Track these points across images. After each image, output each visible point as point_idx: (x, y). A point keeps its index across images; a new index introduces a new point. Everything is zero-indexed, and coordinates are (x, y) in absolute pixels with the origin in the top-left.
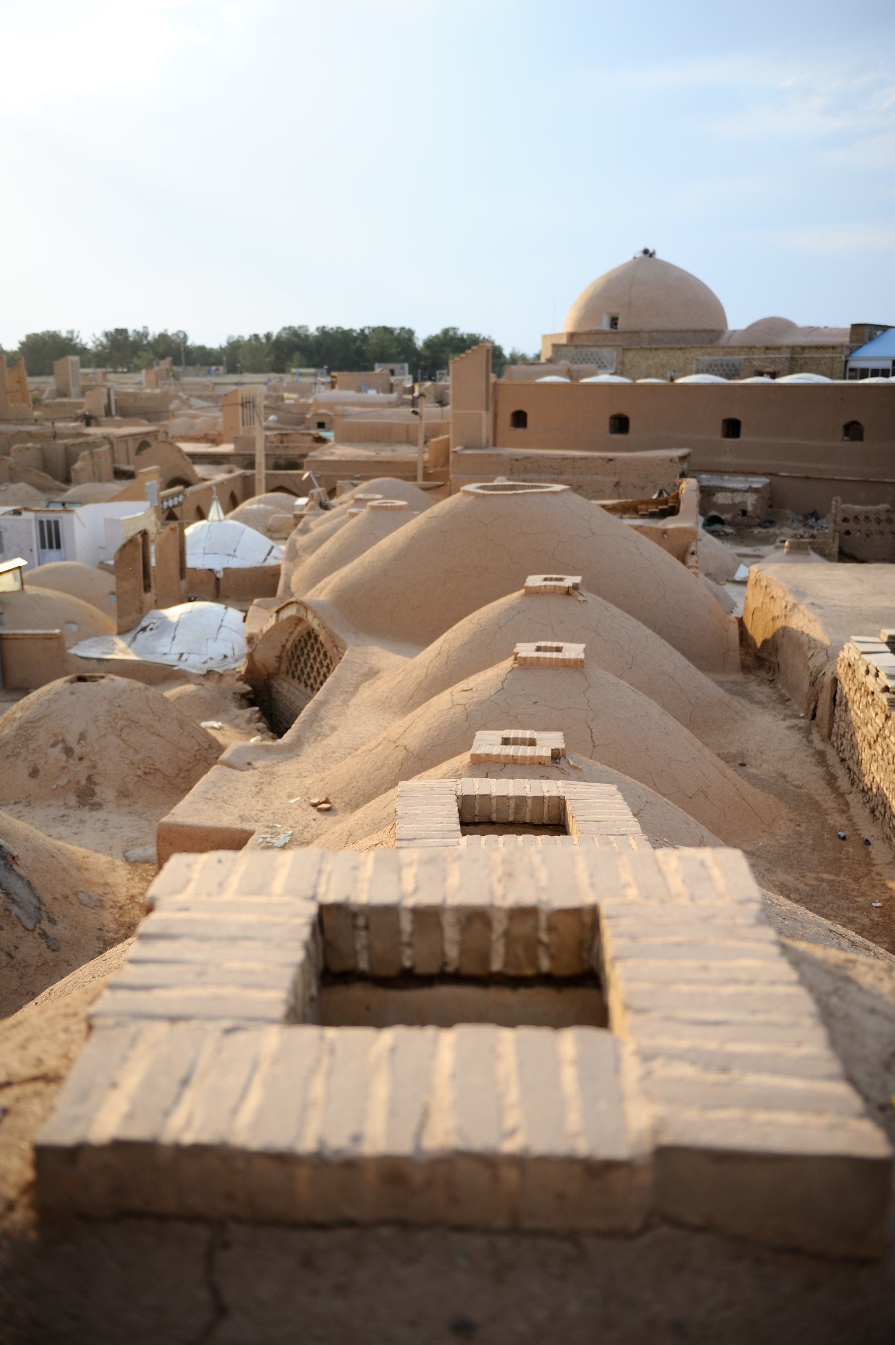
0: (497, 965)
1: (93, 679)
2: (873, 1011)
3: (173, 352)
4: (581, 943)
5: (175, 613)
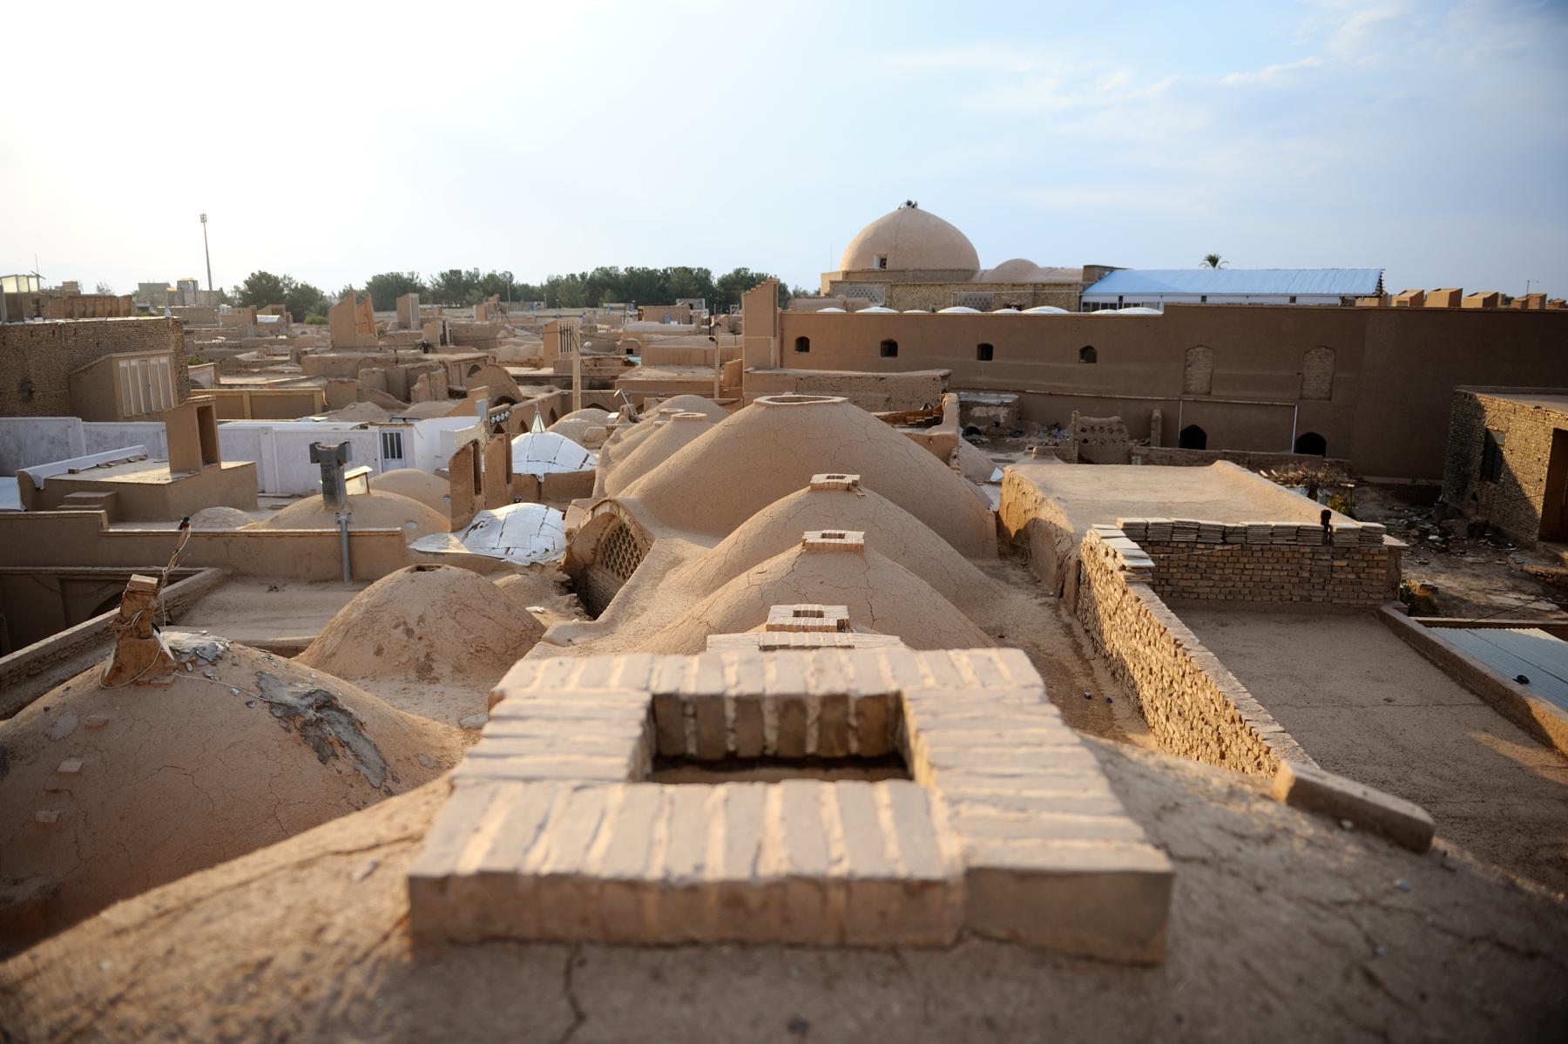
0: (811, 748)
1: (431, 568)
2: (1142, 776)
3: (501, 290)
4: (885, 727)
5: (501, 513)
